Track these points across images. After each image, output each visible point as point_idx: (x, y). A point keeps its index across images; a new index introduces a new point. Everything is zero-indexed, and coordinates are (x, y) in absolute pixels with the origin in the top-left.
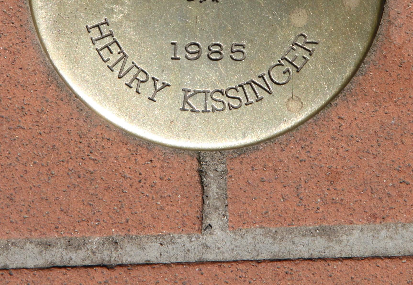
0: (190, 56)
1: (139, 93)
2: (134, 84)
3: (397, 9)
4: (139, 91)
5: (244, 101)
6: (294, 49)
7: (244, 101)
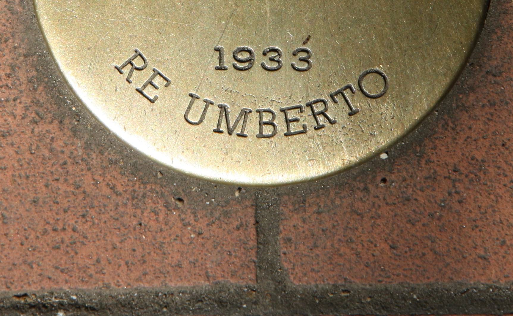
0: (239, 65)
1: (129, 82)
2: (126, 70)
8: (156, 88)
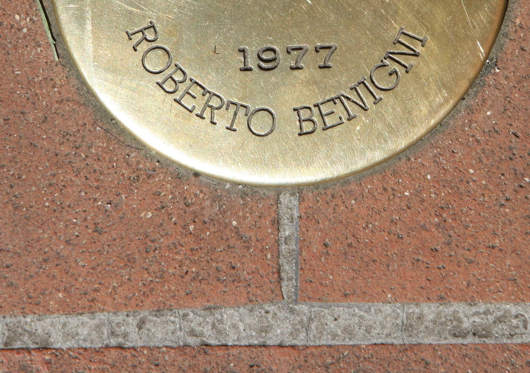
1: (215, 124)
3: (518, 15)
4: (215, 121)
6: (335, 103)
8: (194, 97)
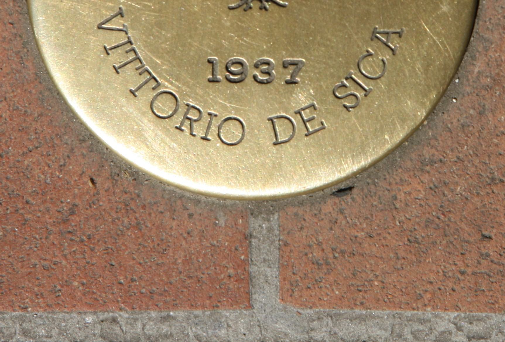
1: (194, 135)
4: (194, 133)
5: (360, 94)
7: (360, 94)
